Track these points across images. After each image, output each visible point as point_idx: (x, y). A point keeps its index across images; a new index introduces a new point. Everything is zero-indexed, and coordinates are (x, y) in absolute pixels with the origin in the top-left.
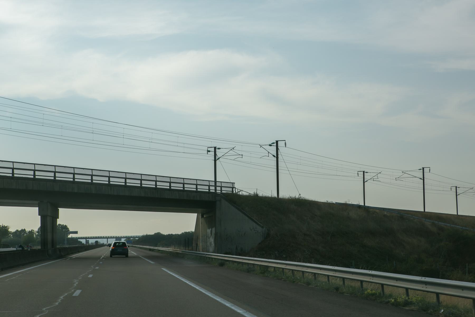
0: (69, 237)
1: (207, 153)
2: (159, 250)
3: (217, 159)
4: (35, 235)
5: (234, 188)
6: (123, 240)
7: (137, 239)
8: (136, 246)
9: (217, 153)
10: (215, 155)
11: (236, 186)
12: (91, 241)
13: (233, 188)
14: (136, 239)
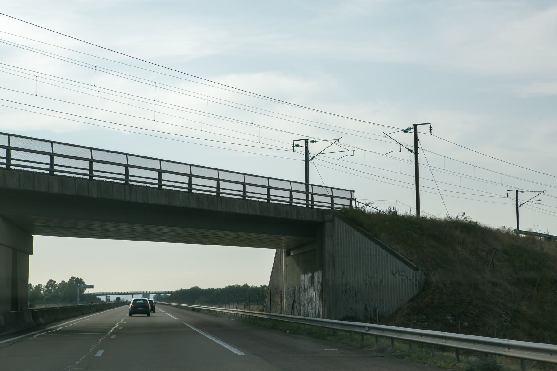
0: (84, 293)
1: (291, 147)
2: (210, 311)
3: (310, 160)
4: (42, 291)
5: (353, 199)
6: (151, 297)
7: (169, 295)
8: (170, 303)
9: (310, 149)
10: (307, 152)
11: (356, 196)
12: (113, 298)
13: (351, 200)
14: (168, 295)
